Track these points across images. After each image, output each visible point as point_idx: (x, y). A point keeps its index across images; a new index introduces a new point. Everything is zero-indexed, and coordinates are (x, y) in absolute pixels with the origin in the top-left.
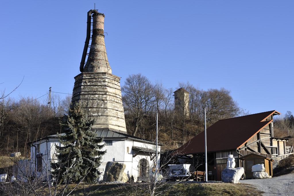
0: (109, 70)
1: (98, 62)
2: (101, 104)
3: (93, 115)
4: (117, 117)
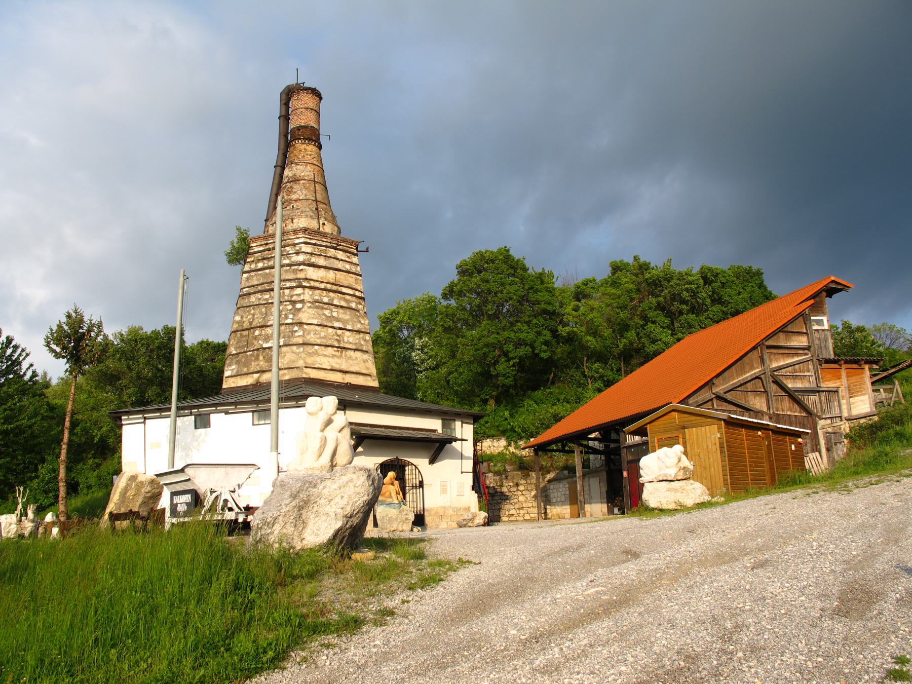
0: (324, 224)
1: (293, 206)
2: (286, 315)
3: (265, 346)
4: (338, 347)
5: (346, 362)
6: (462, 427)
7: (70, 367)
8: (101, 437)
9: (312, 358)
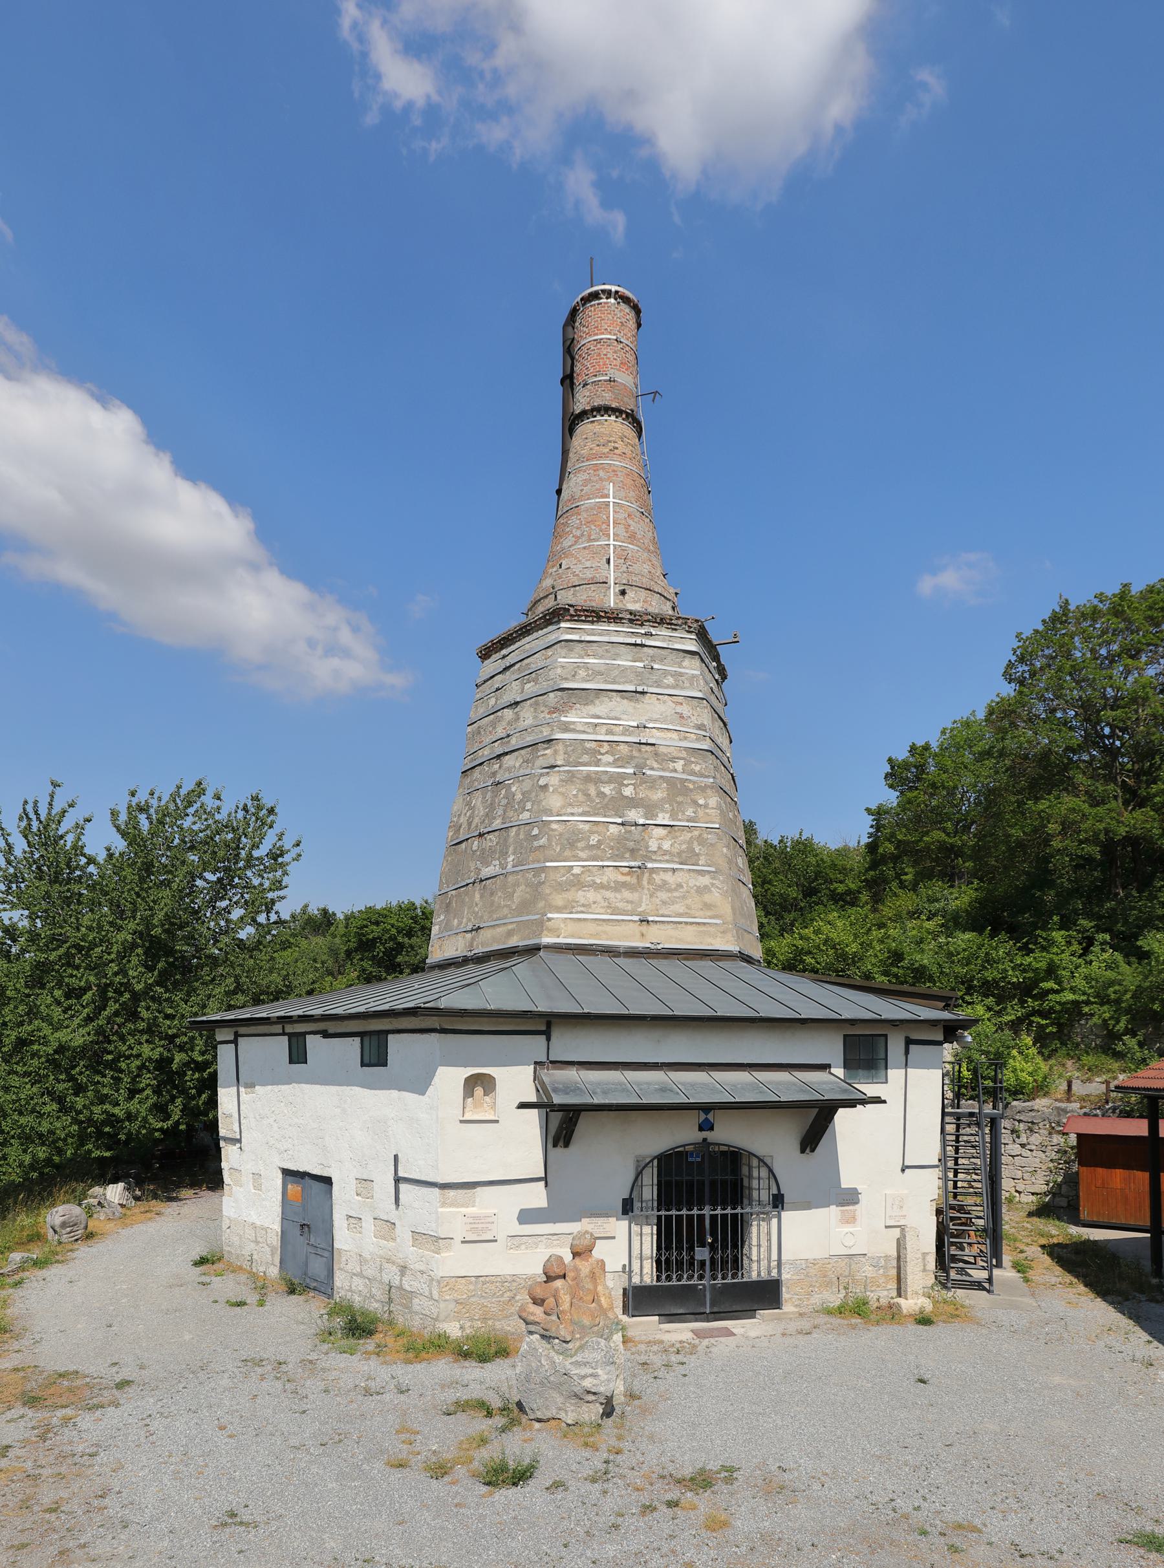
5: (651, 896)
6: (907, 1052)
7: (1066, 924)
8: (992, 939)
9: (565, 895)
